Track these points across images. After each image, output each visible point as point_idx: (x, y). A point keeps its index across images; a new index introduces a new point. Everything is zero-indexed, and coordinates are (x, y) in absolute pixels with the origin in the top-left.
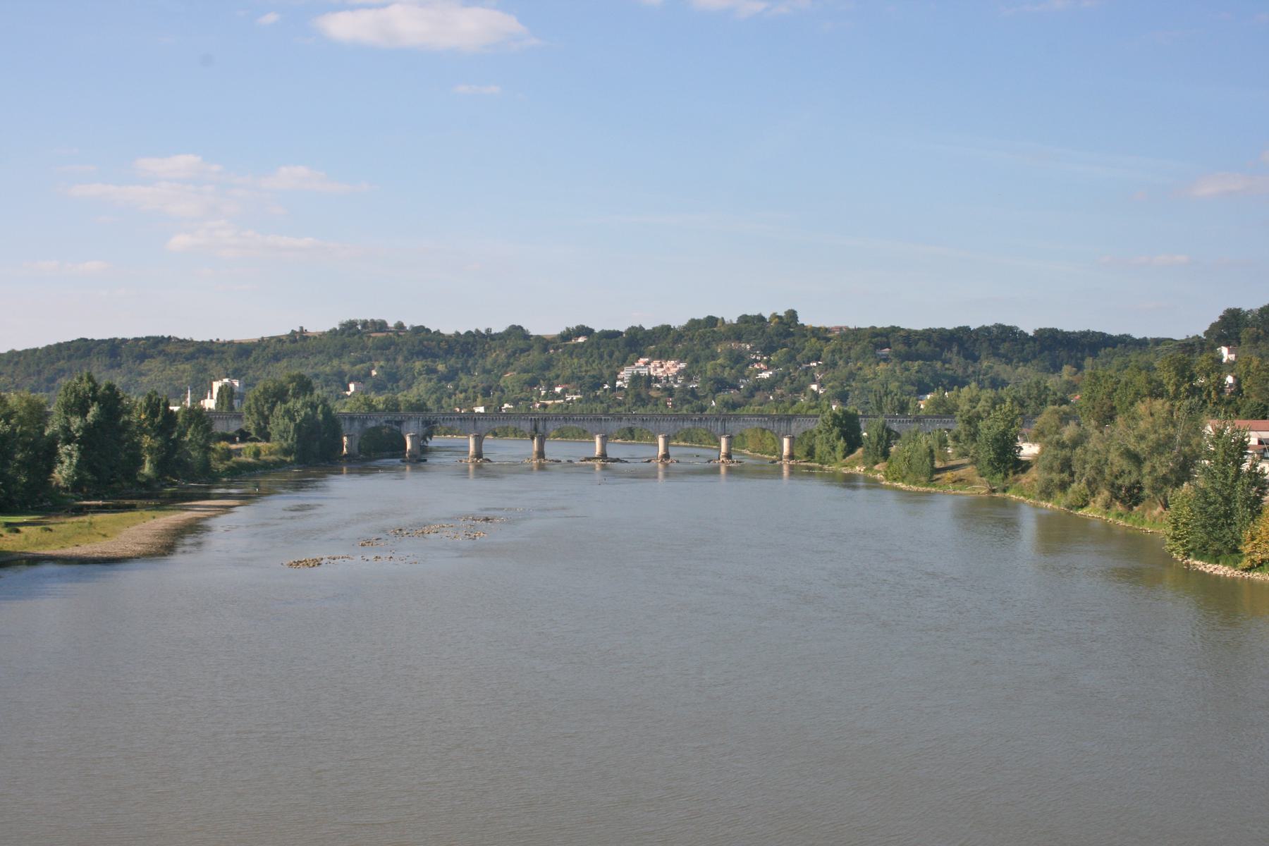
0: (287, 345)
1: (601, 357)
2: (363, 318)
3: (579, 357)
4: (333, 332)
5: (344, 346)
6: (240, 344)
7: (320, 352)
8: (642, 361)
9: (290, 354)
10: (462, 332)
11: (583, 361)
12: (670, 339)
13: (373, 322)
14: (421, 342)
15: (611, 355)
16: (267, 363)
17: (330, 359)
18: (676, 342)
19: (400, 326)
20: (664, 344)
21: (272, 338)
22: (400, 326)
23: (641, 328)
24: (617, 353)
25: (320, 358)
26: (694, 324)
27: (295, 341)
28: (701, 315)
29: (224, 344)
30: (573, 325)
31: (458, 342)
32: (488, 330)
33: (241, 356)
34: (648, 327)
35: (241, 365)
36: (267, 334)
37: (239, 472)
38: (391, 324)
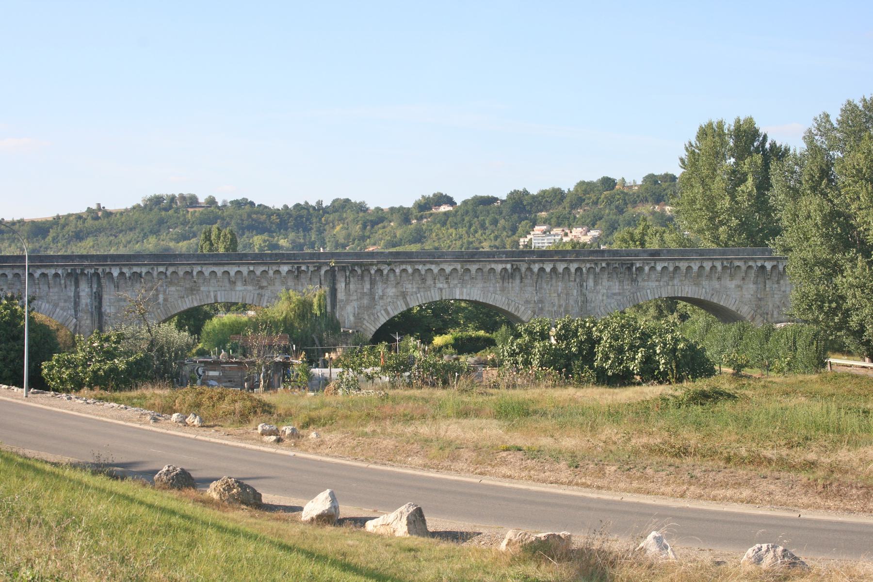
0: (90, 222)
1: (483, 226)
2: (170, 193)
3: (455, 225)
4: (136, 208)
5: (161, 222)
6: (33, 222)
7: (131, 230)
8: (538, 229)
9: (96, 232)
10: (290, 206)
11: (462, 231)
12: (566, 203)
13: (183, 198)
14: (249, 216)
15: (495, 222)
16: (69, 243)
17: (145, 236)
18: (574, 206)
19: (212, 201)
20: (558, 210)
21: (69, 215)
22: (212, 201)
23: (526, 193)
24: (502, 222)
25: (131, 235)
26: (586, 187)
27: (97, 218)
28: (594, 177)
29: (13, 223)
30: (430, 193)
31: (290, 215)
32: (319, 203)
33: (36, 235)
34: (534, 191)
35: (37, 245)
36: (63, 212)
37: (675, 518)
38: (202, 200)
